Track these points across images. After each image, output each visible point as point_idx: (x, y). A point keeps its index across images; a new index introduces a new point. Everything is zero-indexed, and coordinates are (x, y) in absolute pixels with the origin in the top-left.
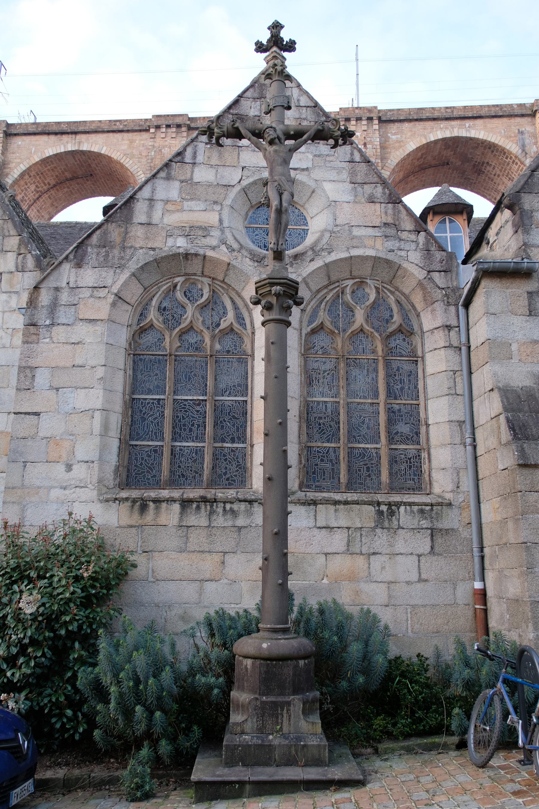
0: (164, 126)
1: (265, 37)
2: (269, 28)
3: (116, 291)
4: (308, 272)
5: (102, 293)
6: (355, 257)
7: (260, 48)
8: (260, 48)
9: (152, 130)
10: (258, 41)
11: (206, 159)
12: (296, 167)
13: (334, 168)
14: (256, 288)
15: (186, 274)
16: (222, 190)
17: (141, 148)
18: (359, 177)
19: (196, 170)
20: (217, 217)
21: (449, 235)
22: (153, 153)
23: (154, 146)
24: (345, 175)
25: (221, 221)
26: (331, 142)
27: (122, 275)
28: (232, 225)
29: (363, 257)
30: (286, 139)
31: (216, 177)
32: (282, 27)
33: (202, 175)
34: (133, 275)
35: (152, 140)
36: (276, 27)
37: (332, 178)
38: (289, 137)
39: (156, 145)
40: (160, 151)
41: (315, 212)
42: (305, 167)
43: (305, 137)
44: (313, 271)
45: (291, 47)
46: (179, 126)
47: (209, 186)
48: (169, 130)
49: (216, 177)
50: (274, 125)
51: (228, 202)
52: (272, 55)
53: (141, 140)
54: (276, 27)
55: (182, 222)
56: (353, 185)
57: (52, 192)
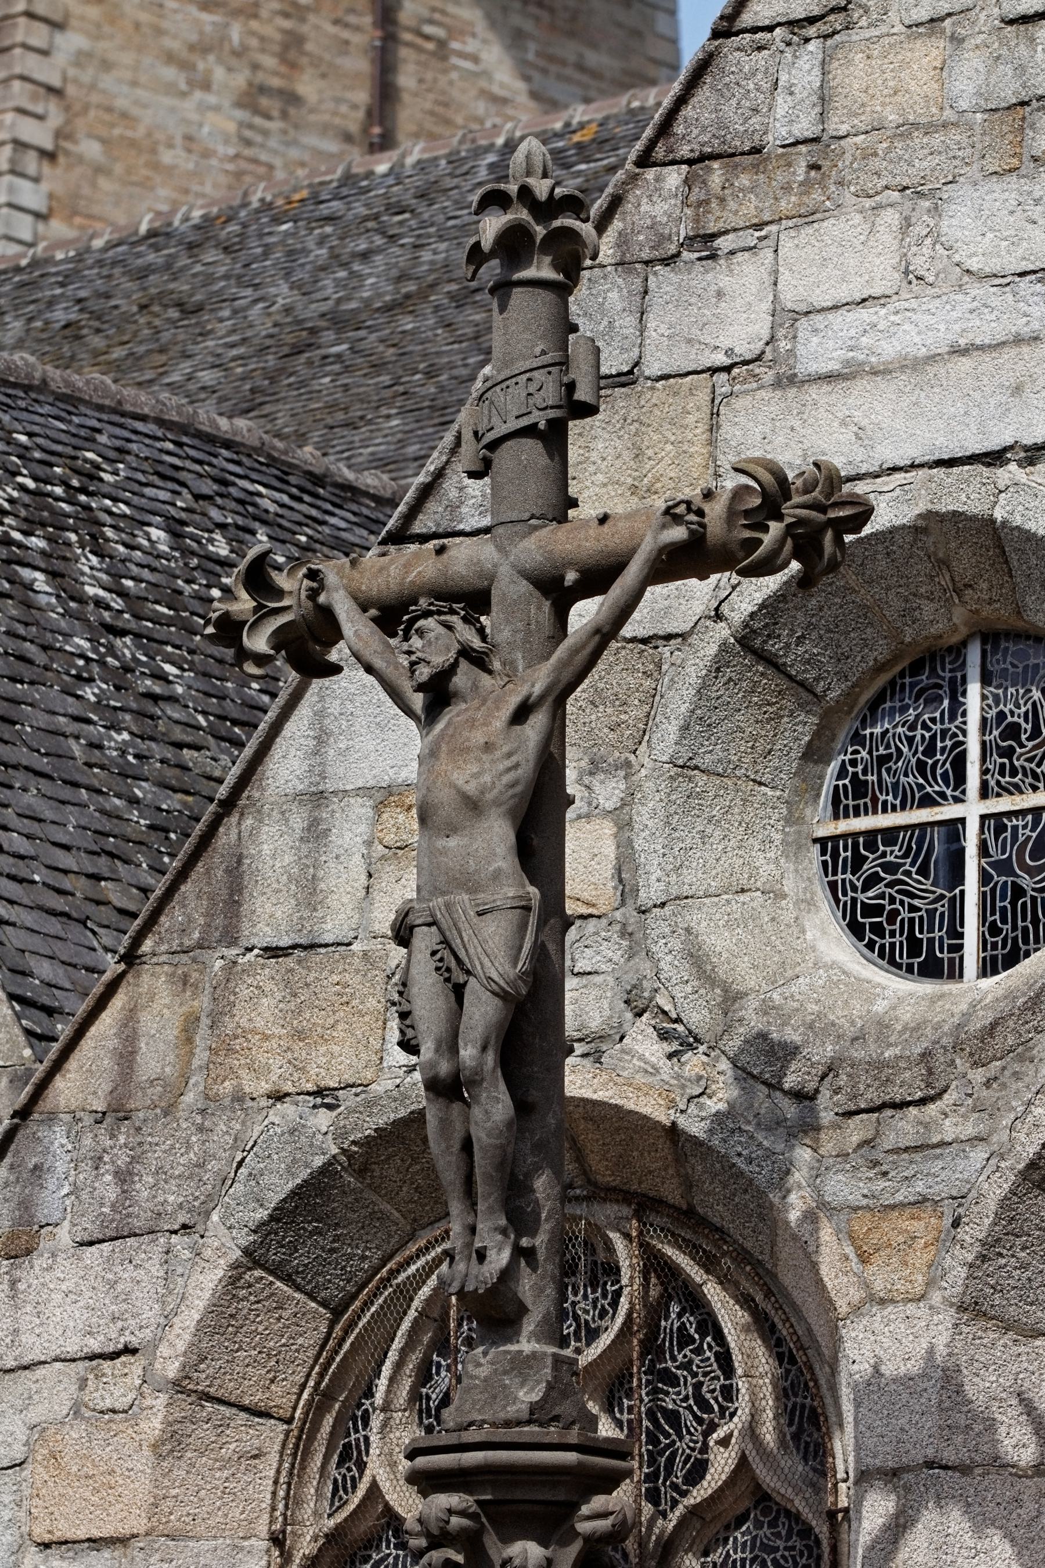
3: (172, 1370)
5: (118, 1386)
12: (993, 444)
21: (972, 810)
27: (197, 1277)
34: (252, 1258)
57: (978, 998)
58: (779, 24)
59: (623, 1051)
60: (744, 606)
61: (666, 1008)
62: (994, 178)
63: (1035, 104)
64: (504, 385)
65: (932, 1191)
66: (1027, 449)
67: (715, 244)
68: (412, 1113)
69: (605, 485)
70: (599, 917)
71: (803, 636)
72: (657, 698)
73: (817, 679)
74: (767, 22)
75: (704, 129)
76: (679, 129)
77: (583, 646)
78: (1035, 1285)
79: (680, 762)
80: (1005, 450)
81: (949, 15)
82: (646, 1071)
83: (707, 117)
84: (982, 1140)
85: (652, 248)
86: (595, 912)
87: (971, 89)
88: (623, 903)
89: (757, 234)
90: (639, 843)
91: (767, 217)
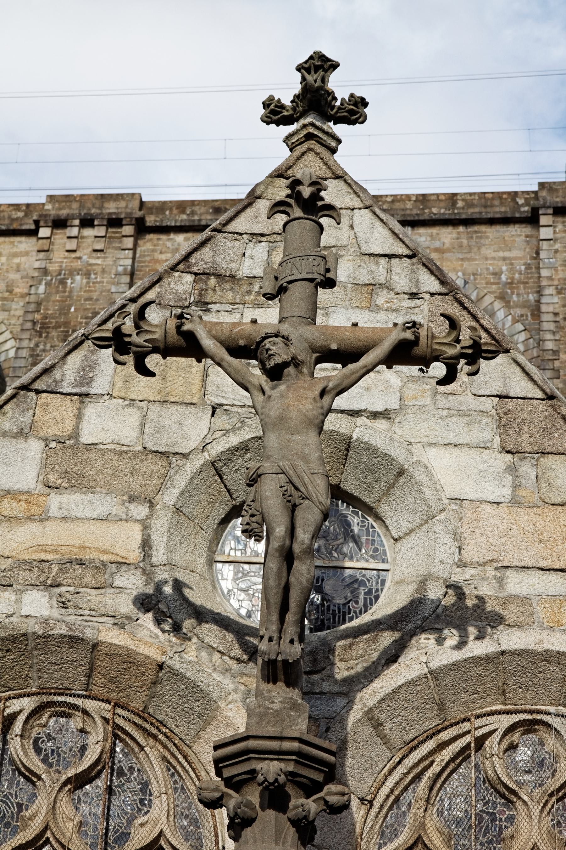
0: (77, 222)
1: (288, 89)
2: (299, 69)
4: (381, 694)
6: (513, 653)
7: (274, 113)
8: (274, 113)
9: (44, 232)
10: (271, 98)
11: (119, 384)
12: (356, 407)
13: (460, 414)
14: (217, 762)
15: (43, 691)
16: (156, 466)
17: (13, 276)
18: (525, 436)
19: (91, 411)
20: (136, 534)
22: (42, 288)
23: (45, 271)
24: (486, 432)
25: (146, 544)
26: (438, 369)
28: (176, 558)
29: (534, 653)
30: (319, 361)
31: (142, 433)
32: (335, 66)
33: (107, 424)
35: (42, 255)
36: (319, 66)
37: (451, 438)
38: (327, 355)
39: (53, 268)
40: (63, 282)
41: (405, 526)
42: (380, 408)
43: (366, 360)
44: (394, 691)
45: (355, 111)
46: (114, 222)
47: (121, 453)
48: (88, 232)
49: (142, 433)
50: (285, 329)
51: (171, 496)
52: (305, 132)
53: (15, 255)
54: (319, 66)
55: (41, 548)
56: (509, 457)
58: (246, 233)
59: (139, 625)
60: (219, 448)
61: (164, 610)
62: (357, 309)
63: (377, 286)
64: (301, 258)
65: (314, 713)
66: (372, 413)
67: (209, 306)
68: (9, 635)
69: (144, 387)
70: (129, 564)
71: (237, 469)
72: (167, 478)
73: (236, 491)
74: (240, 231)
75: (206, 263)
76: (192, 260)
77: (357, 372)
78: (355, 767)
79: (177, 507)
80: (361, 411)
81: (334, 246)
82: (151, 637)
83: (207, 258)
84: (344, 694)
85: (175, 301)
86: (128, 562)
87: (345, 274)
88: (144, 560)
89: (232, 307)
90: (153, 537)
91: (237, 301)
